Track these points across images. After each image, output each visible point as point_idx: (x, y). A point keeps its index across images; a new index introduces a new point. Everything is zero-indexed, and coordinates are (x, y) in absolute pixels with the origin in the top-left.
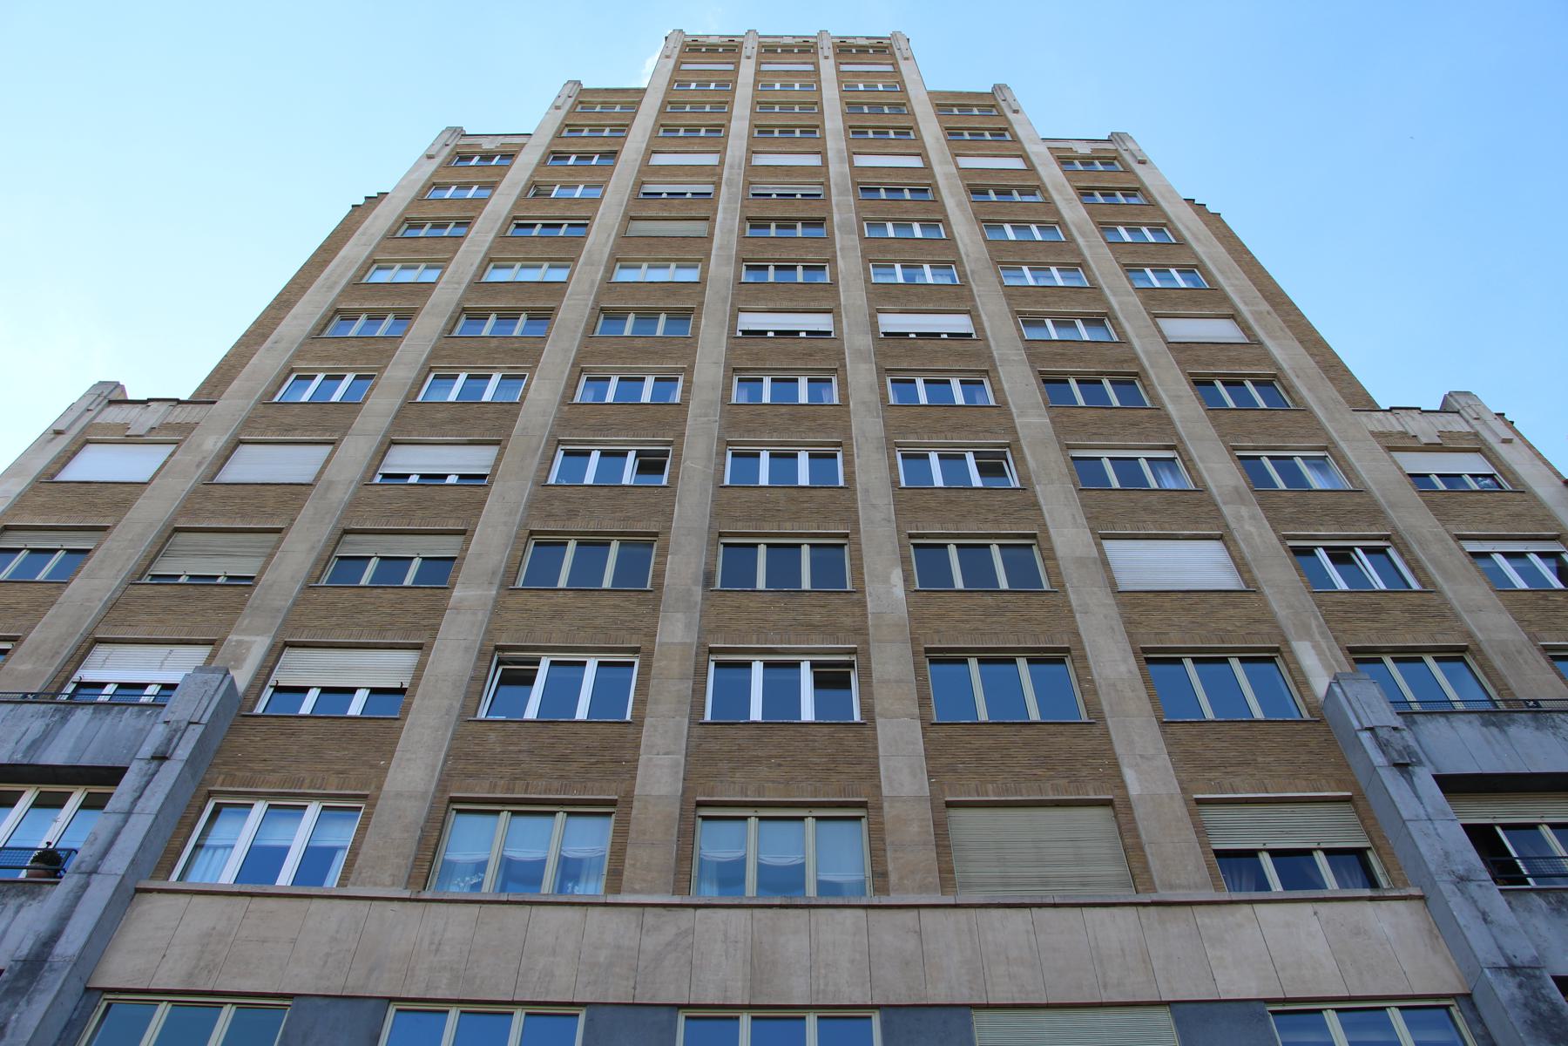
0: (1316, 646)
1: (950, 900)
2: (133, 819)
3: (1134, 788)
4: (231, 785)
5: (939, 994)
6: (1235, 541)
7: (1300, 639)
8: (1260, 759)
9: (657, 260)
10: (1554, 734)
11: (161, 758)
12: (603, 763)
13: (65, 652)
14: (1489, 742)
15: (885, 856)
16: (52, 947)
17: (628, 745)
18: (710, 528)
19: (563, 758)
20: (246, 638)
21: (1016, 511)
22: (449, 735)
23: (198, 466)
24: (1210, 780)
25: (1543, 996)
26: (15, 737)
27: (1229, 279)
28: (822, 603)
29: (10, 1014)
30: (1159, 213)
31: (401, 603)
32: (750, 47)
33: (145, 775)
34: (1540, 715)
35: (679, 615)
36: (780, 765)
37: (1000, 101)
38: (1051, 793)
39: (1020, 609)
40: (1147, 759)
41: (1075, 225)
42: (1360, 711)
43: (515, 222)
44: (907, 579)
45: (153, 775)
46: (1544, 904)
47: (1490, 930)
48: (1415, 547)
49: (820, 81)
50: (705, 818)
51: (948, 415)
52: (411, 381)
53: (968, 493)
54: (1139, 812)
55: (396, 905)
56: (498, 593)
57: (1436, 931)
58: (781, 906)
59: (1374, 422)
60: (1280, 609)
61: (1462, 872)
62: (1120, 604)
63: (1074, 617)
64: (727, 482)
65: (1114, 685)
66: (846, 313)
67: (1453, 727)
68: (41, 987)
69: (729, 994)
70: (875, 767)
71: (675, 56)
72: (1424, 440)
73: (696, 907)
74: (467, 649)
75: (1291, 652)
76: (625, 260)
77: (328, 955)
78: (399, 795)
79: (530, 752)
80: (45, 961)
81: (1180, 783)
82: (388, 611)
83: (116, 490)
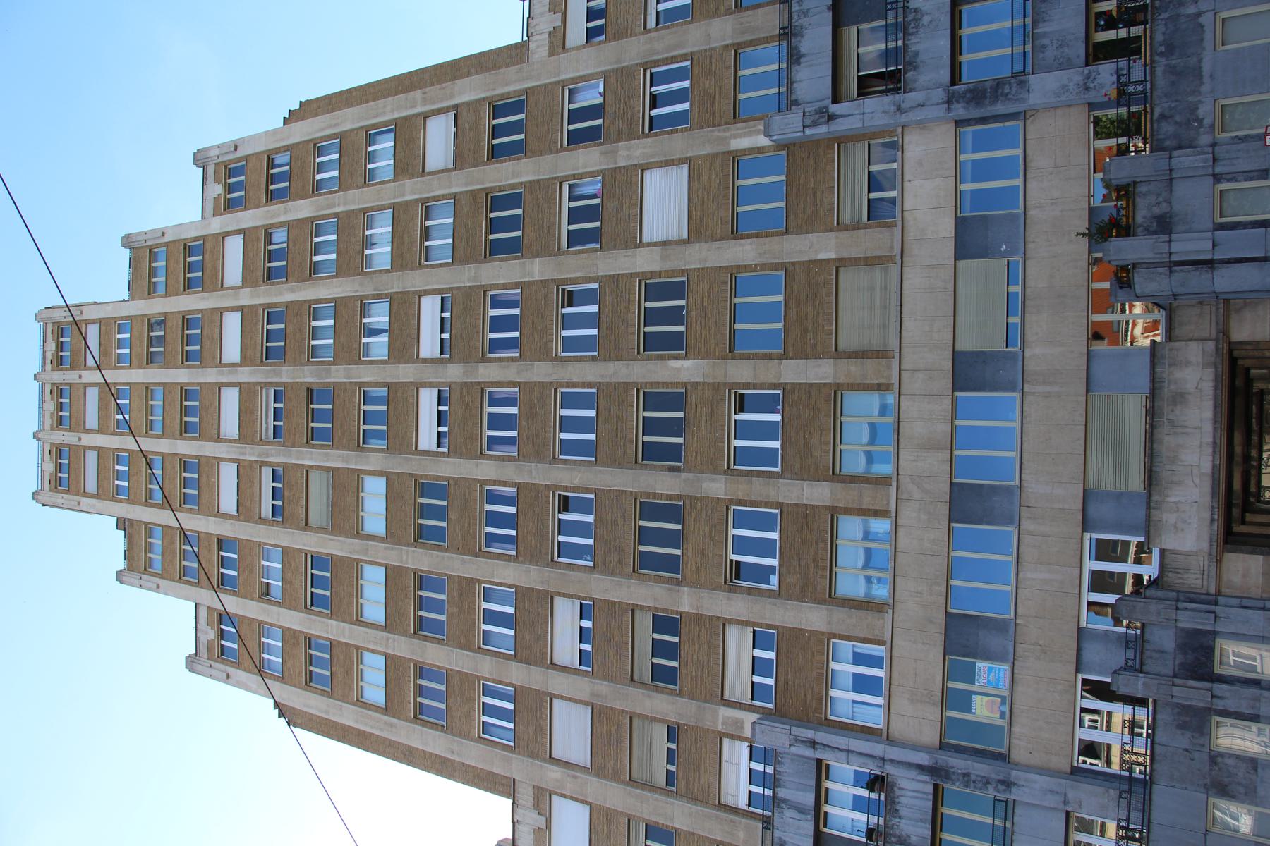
0: (735, 137)
1: (897, 355)
2: (852, 748)
3: (832, 255)
4: (822, 710)
5: (948, 365)
6: (646, 164)
7: (729, 144)
8: (812, 185)
9: (358, 506)
10: (806, 29)
11: (813, 744)
12: (807, 523)
13: (731, 817)
14: (811, 66)
15: (868, 384)
16: (925, 766)
17: (795, 510)
18: (632, 469)
19: (804, 542)
21: (619, 289)
22: (789, 602)
23: (575, 777)
24: (825, 215)
25: (963, 94)
26: (797, 822)
27: (384, 113)
28: (694, 407)
29: (959, 774)
30: (301, 146)
31: (692, 640)
32: (63, 438)
33: (824, 749)
34: (793, 32)
35: (704, 485)
36: (810, 433)
37: (144, 245)
38: (831, 298)
39: (701, 297)
40: (811, 245)
41: (318, 211)
42: (791, 130)
43: (309, 607)
44: (676, 358)
45: (824, 745)
46: (911, 73)
47: (928, 106)
48: (656, 57)
49: (115, 383)
50: (840, 471)
51: (529, 321)
52: (494, 659)
53: (602, 316)
54: (846, 255)
55: (895, 616)
56: (684, 586)
57: (921, 126)
58: (898, 435)
59: (539, 49)
60: (708, 150)
61: (895, 108)
62: (699, 240)
63: (707, 268)
64: (593, 459)
65: (760, 254)
66: (423, 379)
67: (800, 81)
68: (945, 765)
69: (945, 459)
70: (812, 385)
71: (77, 498)
72: (559, 23)
73: (898, 474)
74: (729, 599)
75: (737, 151)
76: (358, 530)
77: (923, 643)
78: (829, 623)
79: (800, 560)
80: (932, 767)
81: (826, 231)
82: (698, 646)
83: (596, 823)
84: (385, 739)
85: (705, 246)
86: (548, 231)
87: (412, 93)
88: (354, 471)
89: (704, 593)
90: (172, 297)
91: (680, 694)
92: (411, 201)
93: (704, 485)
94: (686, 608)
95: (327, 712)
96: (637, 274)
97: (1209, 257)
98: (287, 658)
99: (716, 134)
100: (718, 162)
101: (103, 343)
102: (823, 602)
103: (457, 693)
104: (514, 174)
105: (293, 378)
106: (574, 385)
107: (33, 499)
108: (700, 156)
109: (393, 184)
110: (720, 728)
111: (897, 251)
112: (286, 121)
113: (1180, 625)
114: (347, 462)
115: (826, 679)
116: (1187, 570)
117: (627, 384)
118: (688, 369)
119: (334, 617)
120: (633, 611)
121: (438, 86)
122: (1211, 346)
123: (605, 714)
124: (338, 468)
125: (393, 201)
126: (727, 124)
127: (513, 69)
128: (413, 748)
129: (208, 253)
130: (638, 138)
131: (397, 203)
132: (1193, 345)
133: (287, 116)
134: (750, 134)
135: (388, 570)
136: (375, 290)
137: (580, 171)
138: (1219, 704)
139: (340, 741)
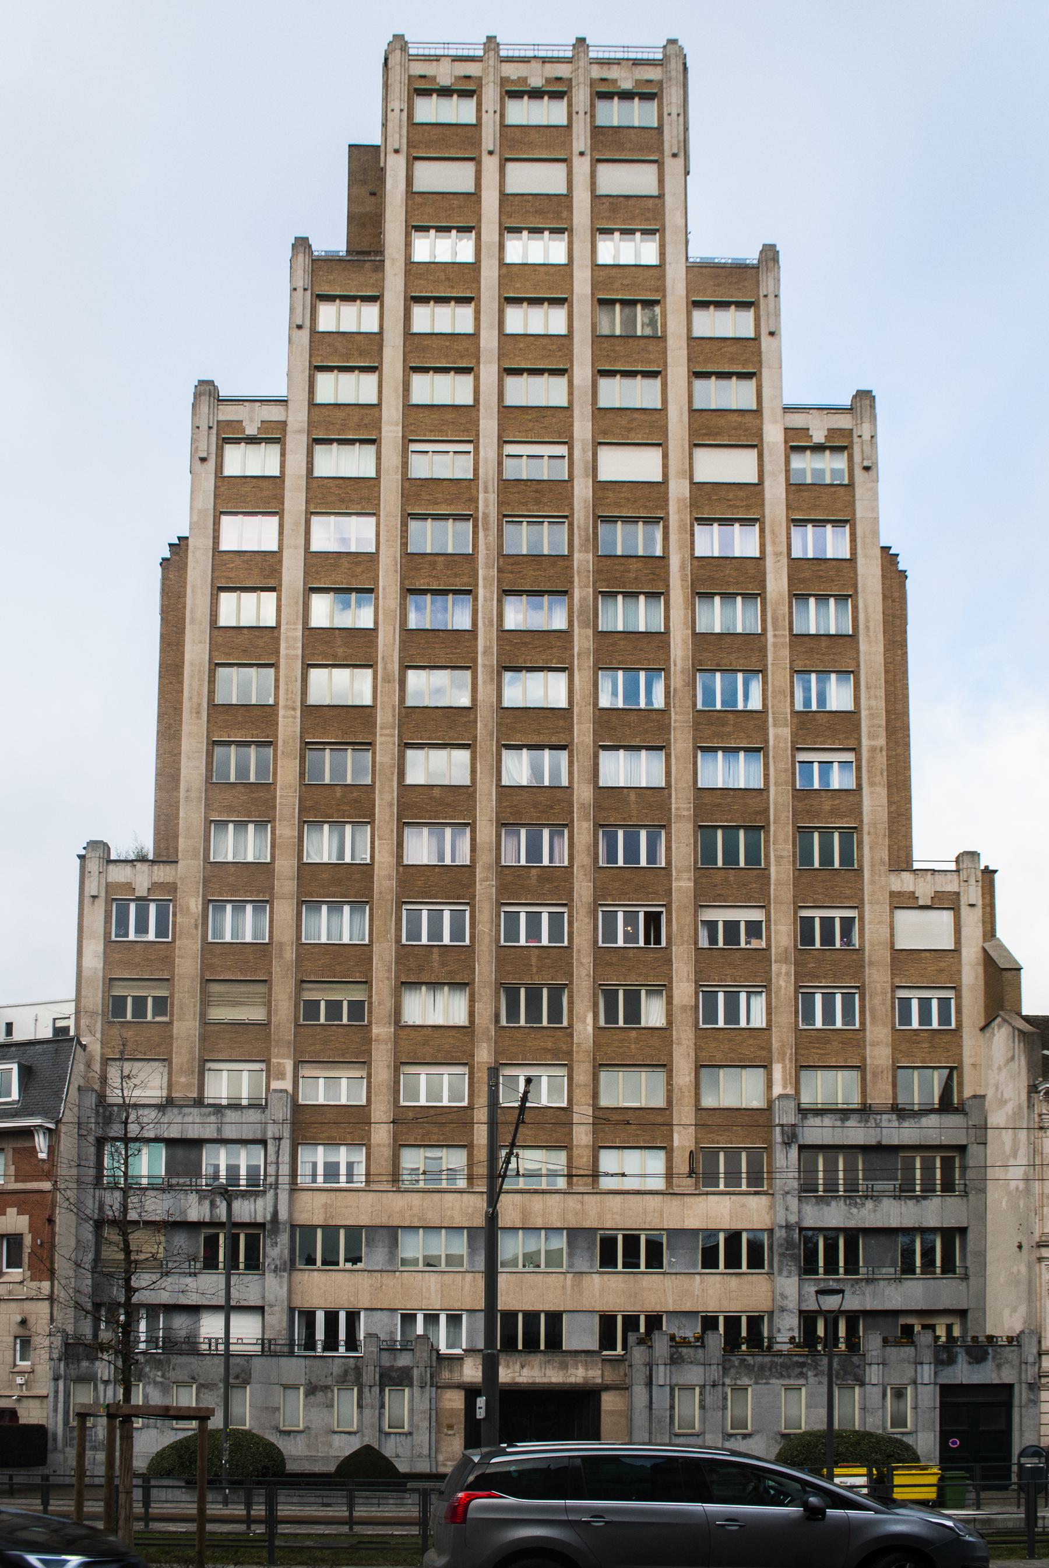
0: (784, 1068)
2: (281, 1166)
3: (676, 1143)
5: (587, 1224)
7: (778, 1062)
20: (281, 1061)
48: (867, 998)
54: (675, 1154)
60: (775, 1044)
72: (921, 903)
78: (379, 1145)
81: (696, 1138)
84: (181, 703)
85: (691, 1043)
86: (719, 895)
87: (884, 734)
88: (475, 660)
89: (390, 1046)
90: (685, 352)
91: (297, 1026)
92: (767, 734)
93: (485, 1045)
94: (375, 1030)
95: (193, 621)
96: (671, 983)
97: (654, 1382)
98: (245, 558)
99: (789, 1052)
100: (764, 1053)
101: (631, 202)
102: (395, 1140)
103: (253, 795)
104: (779, 858)
105: (579, 655)
106: (571, 924)
107: (394, 36)
108: (771, 1037)
109: (789, 711)
110: (274, 1060)
111: (677, 1190)
112: (885, 549)
113: (415, 1369)
114: (485, 652)
115: (332, 1143)
116: (451, 1371)
117: (572, 975)
118: (585, 1029)
119: (306, 633)
120: (366, 982)
121: (885, 767)
122: (599, 1381)
123: (264, 956)
124: (476, 639)
125: (770, 711)
126: (796, 1060)
127: (885, 855)
128: (180, 739)
129: (739, 419)
130: (796, 982)
131: (767, 716)
132: (600, 1372)
133: (891, 552)
134: (784, 1080)
135: (369, 710)
136: (675, 690)
137: (773, 927)
138: (366, 1390)
139: (163, 636)
